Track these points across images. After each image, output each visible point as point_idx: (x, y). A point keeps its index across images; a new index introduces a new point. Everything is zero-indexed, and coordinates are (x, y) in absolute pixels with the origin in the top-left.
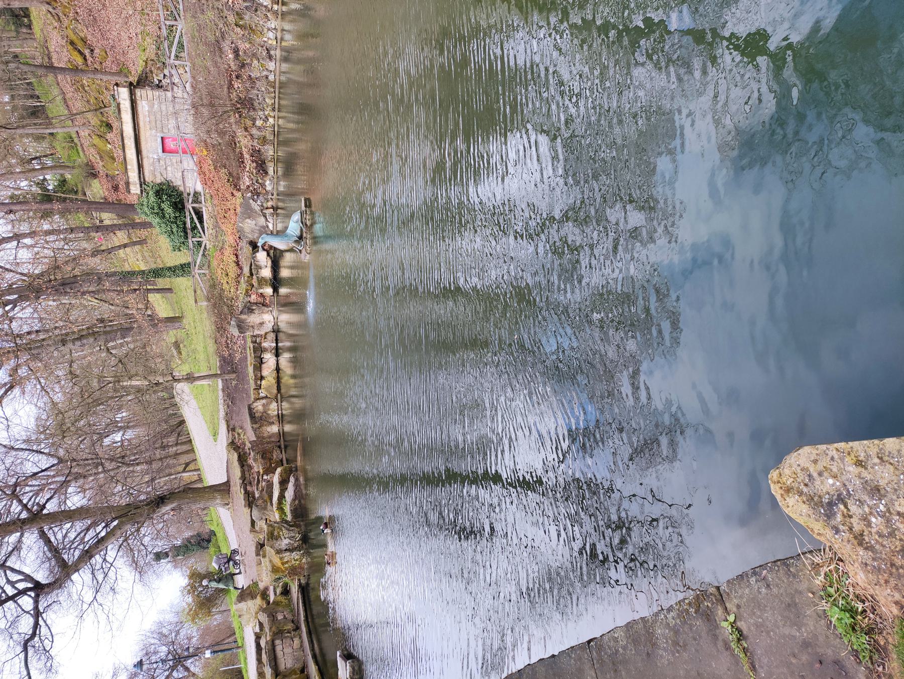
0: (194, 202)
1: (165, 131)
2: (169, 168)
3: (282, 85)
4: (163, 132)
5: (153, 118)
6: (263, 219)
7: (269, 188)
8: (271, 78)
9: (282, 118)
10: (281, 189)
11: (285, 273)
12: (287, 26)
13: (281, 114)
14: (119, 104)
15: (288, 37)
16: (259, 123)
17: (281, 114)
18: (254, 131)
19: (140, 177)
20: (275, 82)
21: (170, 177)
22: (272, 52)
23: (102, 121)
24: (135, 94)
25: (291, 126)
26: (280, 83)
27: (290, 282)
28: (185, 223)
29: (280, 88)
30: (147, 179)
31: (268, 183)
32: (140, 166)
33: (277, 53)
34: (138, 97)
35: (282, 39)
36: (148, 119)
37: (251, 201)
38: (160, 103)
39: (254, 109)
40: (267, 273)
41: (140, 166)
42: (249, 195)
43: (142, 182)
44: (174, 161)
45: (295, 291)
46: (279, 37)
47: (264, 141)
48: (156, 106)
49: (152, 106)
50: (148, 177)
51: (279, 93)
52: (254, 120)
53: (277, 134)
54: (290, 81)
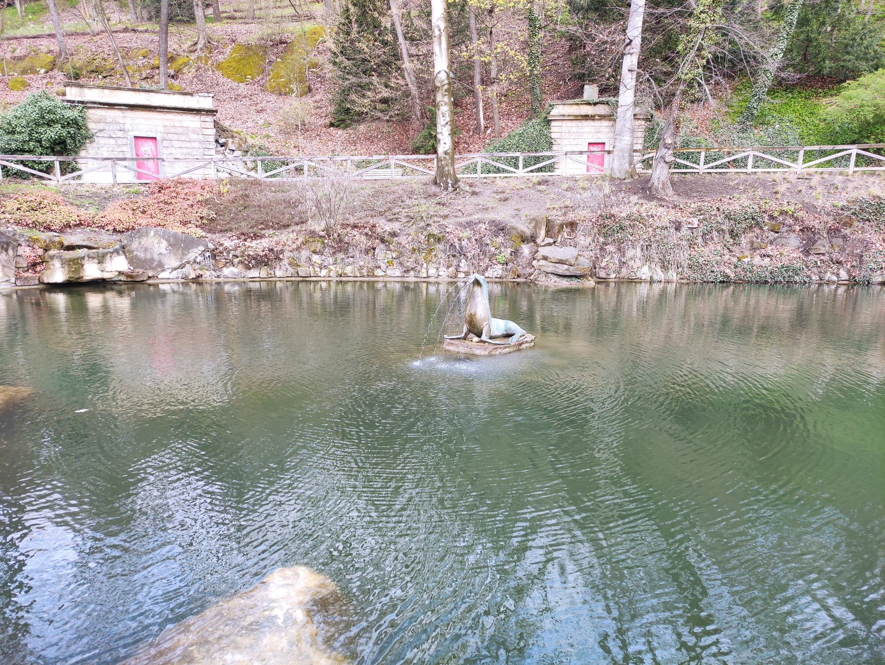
0: (475, 171)
1: (165, 143)
2: (112, 141)
3: (371, 285)
4: (163, 140)
5: (180, 130)
6: (176, 264)
7: (227, 271)
8: (378, 272)
9: (329, 286)
10: (227, 288)
11: (94, 300)
12: (443, 288)
13: (333, 285)
14: (191, 94)
15: (432, 289)
16: (316, 258)
17: (333, 285)
18: (305, 253)
19: (95, 103)
20: (374, 276)
21: (99, 141)
22: (412, 273)
23: (81, 69)
24: (207, 115)
25: (318, 295)
26: (374, 282)
27: (79, 310)
28: (30, 151)
29: (368, 282)
30: (91, 111)
31: (235, 270)
32: (111, 106)
33: (411, 278)
34: (203, 118)
35: (428, 283)
36: (177, 124)
37: (202, 248)
38: (200, 142)
39: (334, 253)
40: (91, 271)
41: (111, 106)
42: (211, 246)
43: (85, 105)
44: (125, 149)
45: (63, 316)
46: (431, 280)
47: (294, 264)
48: (195, 136)
49: (194, 131)
50: (93, 114)
51: (355, 282)
52: (320, 253)
53: (306, 280)
54: (376, 291)
